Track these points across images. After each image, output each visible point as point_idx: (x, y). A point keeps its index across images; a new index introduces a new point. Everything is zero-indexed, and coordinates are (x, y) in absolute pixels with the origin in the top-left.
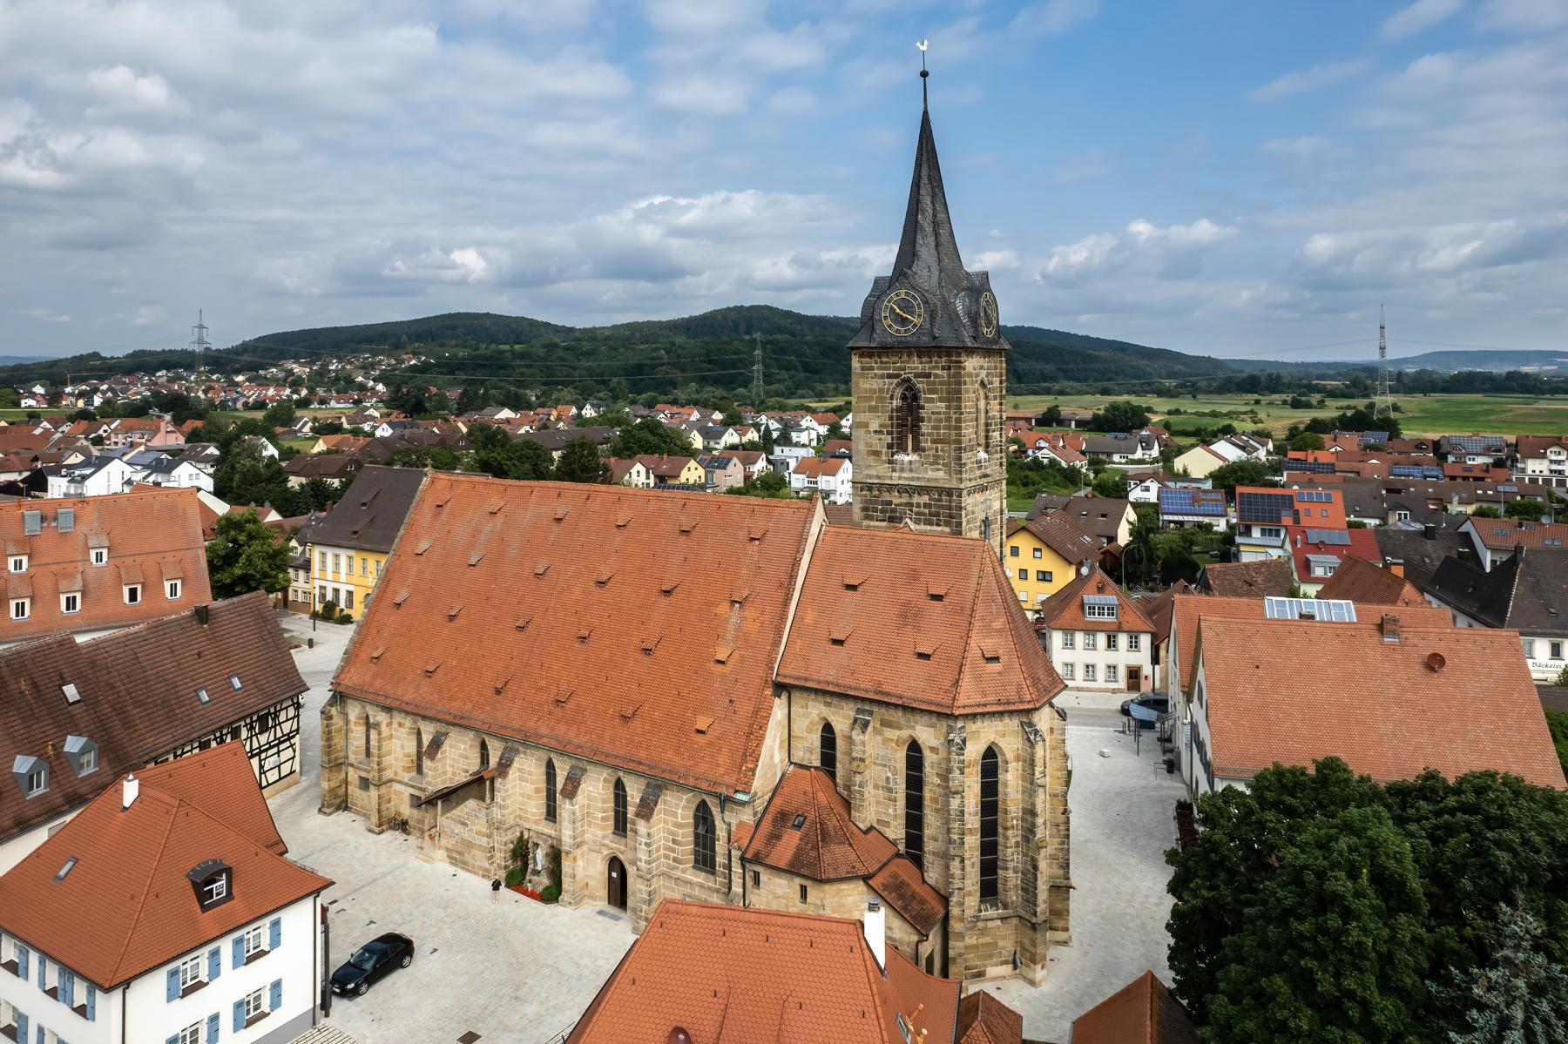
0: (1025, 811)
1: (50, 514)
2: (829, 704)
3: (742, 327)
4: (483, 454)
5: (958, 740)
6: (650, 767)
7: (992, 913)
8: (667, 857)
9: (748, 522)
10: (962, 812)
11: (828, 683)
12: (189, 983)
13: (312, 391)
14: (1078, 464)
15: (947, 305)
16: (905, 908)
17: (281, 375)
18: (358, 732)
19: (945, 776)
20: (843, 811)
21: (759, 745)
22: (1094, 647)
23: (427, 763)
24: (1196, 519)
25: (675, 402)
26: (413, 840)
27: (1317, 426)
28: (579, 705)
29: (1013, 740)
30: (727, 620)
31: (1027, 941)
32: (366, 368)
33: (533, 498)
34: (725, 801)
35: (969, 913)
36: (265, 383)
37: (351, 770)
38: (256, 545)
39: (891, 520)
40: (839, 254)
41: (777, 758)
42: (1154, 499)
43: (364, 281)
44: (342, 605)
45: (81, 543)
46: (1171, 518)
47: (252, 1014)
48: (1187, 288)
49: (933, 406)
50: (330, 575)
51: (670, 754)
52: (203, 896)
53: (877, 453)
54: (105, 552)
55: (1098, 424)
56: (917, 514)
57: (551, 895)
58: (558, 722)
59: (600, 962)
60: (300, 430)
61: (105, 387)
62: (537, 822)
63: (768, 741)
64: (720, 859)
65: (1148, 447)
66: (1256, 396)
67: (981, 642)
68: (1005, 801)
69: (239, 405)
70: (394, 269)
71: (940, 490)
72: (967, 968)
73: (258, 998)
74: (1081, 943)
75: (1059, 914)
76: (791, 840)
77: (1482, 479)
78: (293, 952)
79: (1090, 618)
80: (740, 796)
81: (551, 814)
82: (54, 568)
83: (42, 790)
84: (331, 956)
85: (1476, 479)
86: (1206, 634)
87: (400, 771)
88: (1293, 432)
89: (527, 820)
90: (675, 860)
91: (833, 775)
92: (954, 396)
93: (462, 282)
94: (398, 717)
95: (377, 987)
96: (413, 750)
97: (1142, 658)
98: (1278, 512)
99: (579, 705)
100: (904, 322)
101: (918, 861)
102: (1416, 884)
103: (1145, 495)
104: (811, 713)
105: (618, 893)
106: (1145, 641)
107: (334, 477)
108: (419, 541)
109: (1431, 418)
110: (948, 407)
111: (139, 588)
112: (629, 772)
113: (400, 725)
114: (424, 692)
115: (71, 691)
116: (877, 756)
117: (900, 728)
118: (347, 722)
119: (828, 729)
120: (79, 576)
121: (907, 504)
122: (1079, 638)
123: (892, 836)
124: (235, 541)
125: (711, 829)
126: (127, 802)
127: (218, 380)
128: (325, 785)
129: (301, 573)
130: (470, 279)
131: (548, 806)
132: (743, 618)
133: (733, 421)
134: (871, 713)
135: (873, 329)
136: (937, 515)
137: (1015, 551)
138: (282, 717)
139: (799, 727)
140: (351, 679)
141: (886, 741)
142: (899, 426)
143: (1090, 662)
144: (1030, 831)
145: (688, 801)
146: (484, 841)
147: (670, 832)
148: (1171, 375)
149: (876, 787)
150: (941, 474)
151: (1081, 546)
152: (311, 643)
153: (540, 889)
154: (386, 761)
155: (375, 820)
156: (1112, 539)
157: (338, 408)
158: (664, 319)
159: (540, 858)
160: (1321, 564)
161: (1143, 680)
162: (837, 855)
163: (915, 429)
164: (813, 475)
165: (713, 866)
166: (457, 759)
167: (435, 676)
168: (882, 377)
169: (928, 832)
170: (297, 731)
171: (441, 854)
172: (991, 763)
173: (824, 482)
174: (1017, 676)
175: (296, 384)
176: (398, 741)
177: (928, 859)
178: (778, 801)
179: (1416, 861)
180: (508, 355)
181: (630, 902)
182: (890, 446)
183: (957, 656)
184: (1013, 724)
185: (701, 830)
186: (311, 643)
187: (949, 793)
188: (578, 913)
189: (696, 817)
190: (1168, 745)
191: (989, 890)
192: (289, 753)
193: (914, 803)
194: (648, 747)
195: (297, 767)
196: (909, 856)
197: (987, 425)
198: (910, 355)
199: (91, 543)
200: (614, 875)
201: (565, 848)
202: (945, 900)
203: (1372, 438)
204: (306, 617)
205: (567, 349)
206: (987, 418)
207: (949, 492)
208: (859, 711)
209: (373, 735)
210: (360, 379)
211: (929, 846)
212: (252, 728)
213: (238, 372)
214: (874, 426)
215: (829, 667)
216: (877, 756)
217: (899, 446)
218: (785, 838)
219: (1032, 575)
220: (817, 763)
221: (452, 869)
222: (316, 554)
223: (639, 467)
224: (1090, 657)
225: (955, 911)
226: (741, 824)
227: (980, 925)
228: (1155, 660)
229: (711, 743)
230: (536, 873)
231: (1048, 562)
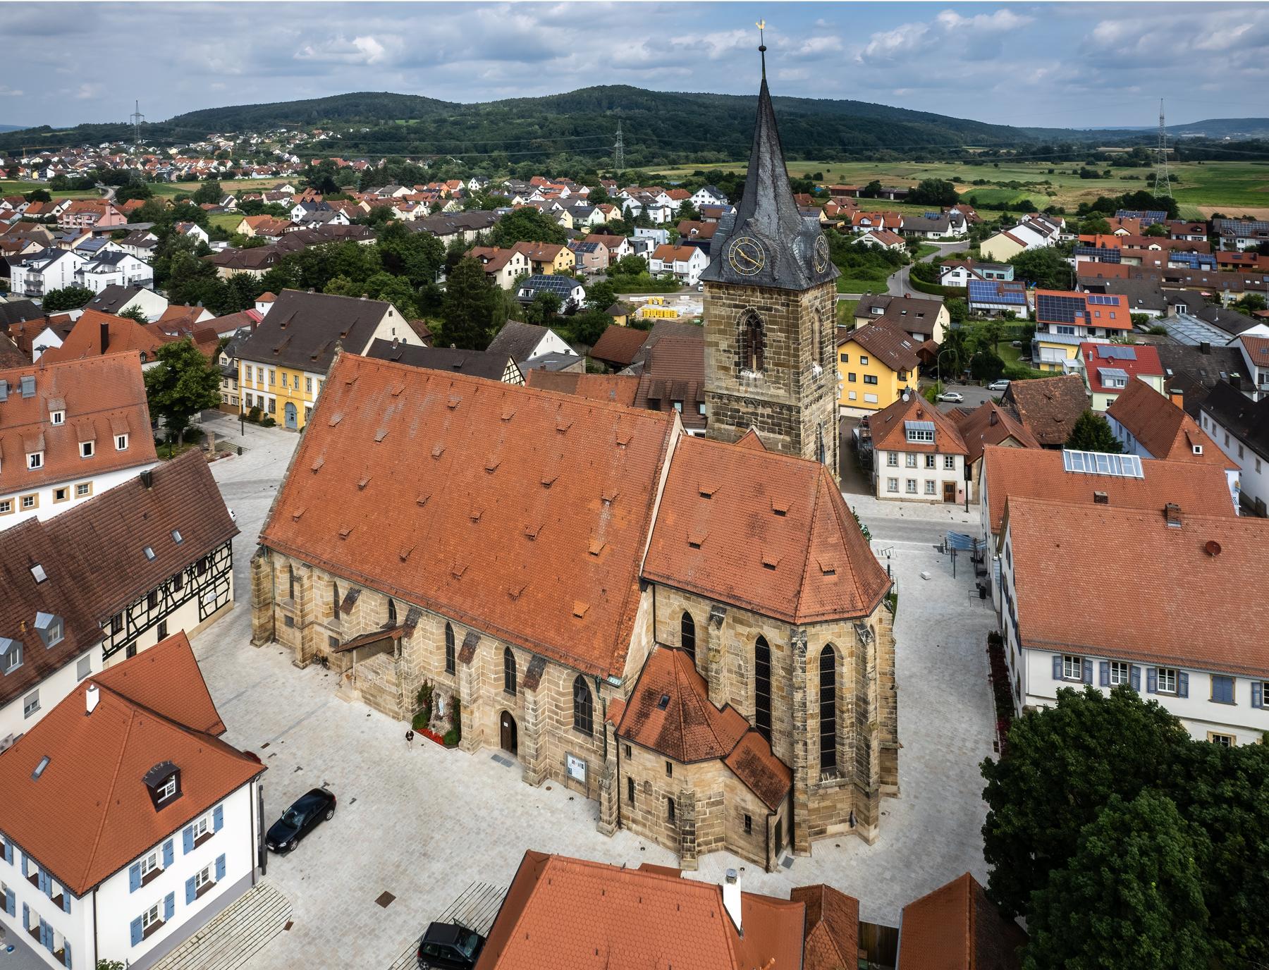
0: (858, 698)
1: (15, 382)
2: (688, 599)
3: (605, 103)
4: (384, 245)
5: (800, 644)
6: (536, 645)
7: (831, 781)
8: (551, 718)
9: (615, 427)
10: (804, 704)
11: (688, 583)
12: (148, 872)
13: (236, 163)
14: (896, 245)
15: (784, 249)
16: (756, 785)
17: (209, 148)
18: (283, 580)
19: (790, 670)
20: (701, 691)
21: (629, 635)
22: (915, 466)
23: (342, 615)
24: (1000, 307)
25: (547, 174)
26: (333, 676)
27: (1104, 206)
29: (848, 639)
31: (861, 804)
32: (283, 142)
33: (430, 386)
34: (599, 683)
35: (811, 782)
36: (195, 155)
37: (277, 609)
38: (191, 371)
39: (739, 425)
40: (688, 39)
41: (644, 641)
42: (963, 284)
43: (276, 62)
44: (266, 410)
45: (42, 405)
46: (979, 306)
47: (201, 885)
48: (989, 67)
49: (774, 335)
50: (255, 385)
51: (552, 634)
52: (155, 796)
53: (726, 369)
54: (62, 414)
55: (912, 198)
56: (762, 422)
57: (452, 739)
59: (496, 813)
60: (226, 206)
61: (56, 159)
62: (439, 674)
63: (636, 630)
64: (597, 727)
65: (959, 225)
66: (1049, 165)
67: (820, 557)
68: (841, 689)
69: (173, 178)
70: (304, 53)
71: (782, 406)
72: (810, 827)
73: (205, 871)
74: (908, 796)
75: (889, 771)
76: (658, 718)
77: (1251, 266)
78: (236, 824)
79: (911, 441)
80: (612, 680)
81: (451, 668)
82: (19, 430)
83: (18, 665)
84: (265, 807)
85: (1244, 265)
86: (1013, 513)
87: (320, 615)
88: (1083, 210)
89: (430, 671)
91: (692, 655)
92: (792, 328)
93: (363, 64)
94: (317, 572)
95: (305, 841)
96: (331, 599)
97: (957, 475)
98: (1072, 314)
99: (472, 580)
100: (748, 264)
101: (767, 735)
102: (1197, 895)
103: (956, 279)
104: (672, 606)
105: (510, 738)
106: (959, 462)
107: (256, 268)
108: (331, 414)
109: (1207, 190)
110: (787, 338)
111: (93, 443)
112: (519, 647)
113: (319, 578)
114: (340, 552)
115: (38, 572)
116: (730, 647)
117: (750, 626)
118: (274, 570)
119: (687, 617)
120: (41, 437)
121: (752, 414)
122: (902, 458)
123: (744, 713)
124: (173, 367)
125: (588, 699)
126: (90, 708)
127: (154, 153)
128: (256, 622)
129: (230, 381)
130: (370, 61)
131: (448, 661)
132: (613, 515)
133: (598, 199)
134: (724, 611)
135: (721, 267)
136: (779, 425)
137: (845, 358)
138: (218, 558)
139: (663, 613)
140: (276, 535)
141: (738, 635)
142: (745, 347)
143: (911, 477)
144: (862, 716)
145: (568, 675)
146: (394, 689)
147: (553, 699)
148: (976, 143)
149: (730, 671)
150: (781, 392)
151: (901, 352)
152: (240, 451)
153: (442, 733)
154: (308, 608)
155: (299, 656)
156: (928, 336)
157: (259, 177)
158: (538, 96)
159: (442, 706)
160: (1110, 377)
161: (957, 494)
162: (698, 734)
163: (760, 346)
165: (591, 729)
166: (369, 614)
167: (348, 540)
168: (729, 306)
169: (775, 714)
170: (231, 567)
171: (356, 694)
172: (828, 658)
173: (678, 266)
174: (850, 587)
175: (222, 157)
176: (318, 593)
177: (775, 736)
178: (645, 679)
179: (1197, 859)
180: (404, 131)
181: (520, 749)
182: (737, 364)
183: (798, 569)
184: (848, 627)
185: (580, 700)
186: (240, 451)
187: (792, 688)
188: (475, 758)
189: (575, 687)
190: (980, 566)
191: (829, 761)
192: (225, 586)
193: (763, 686)
194: (533, 625)
195: (231, 597)
196: (759, 729)
197: (821, 343)
198: (753, 290)
199: (51, 405)
200: (506, 725)
201: (463, 703)
202: (791, 773)
203: (1154, 217)
204: (235, 418)
205: (455, 123)
206: (821, 337)
207: (790, 408)
208: (714, 608)
209: (296, 587)
210: (277, 152)
211: (776, 725)
212: (192, 572)
213: (171, 145)
214: (724, 345)
215: (688, 567)
216: (730, 647)
217: (744, 364)
218: (653, 716)
219: (860, 379)
220: (679, 644)
222: (242, 367)
223: (518, 255)
224: (911, 473)
225: (799, 785)
226: (614, 701)
227: (821, 792)
228: (968, 477)
229: (587, 628)
230: (439, 718)
231: (874, 368)
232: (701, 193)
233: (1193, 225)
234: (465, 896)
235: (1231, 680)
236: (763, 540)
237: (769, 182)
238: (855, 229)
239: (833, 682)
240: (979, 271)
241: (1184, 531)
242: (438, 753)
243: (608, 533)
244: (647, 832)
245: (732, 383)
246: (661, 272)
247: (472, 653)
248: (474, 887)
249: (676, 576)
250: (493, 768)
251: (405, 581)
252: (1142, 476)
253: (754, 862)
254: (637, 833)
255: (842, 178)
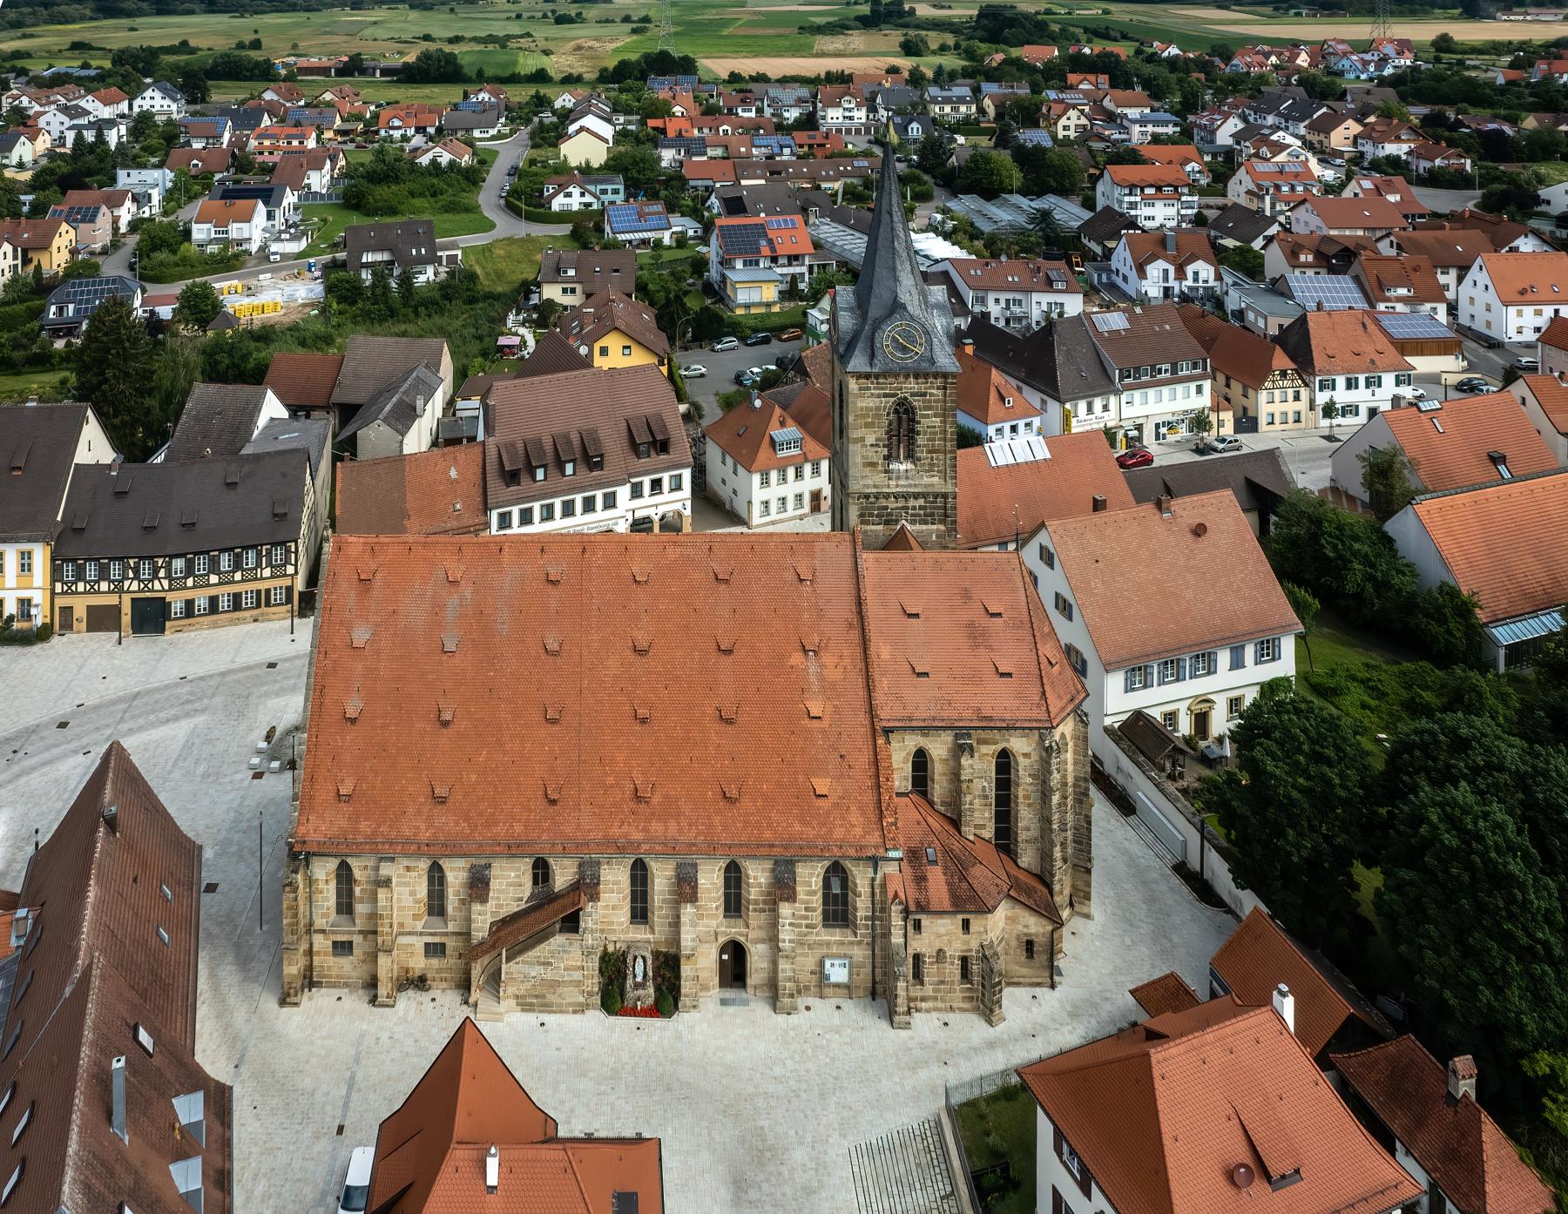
2: (926, 735)
28: (667, 797)
30: (805, 670)
31: (1080, 884)
39: (887, 523)
51: (797, 827)
53: (873, 465)
58: (648, 821)
59: (789, 1063)
71: (936, 495)
79: (780, 454)
90: (807, 926)
99: (667, 797)
100: (904, 349)
103: (567, 200)
104: (912, 742)
110: (944, 422)
132: (822, 666)
134: (969, 736)
153: (650, 1001)
163: (912, 433)
164: (222, 223)
168: (878, 396)
171: (508, 1003)
173: (236, 230)
194: (770, 826)
198: (907, 377)
207: (945, 496)
214: (871, 439)
221: (532, 1019)
229: (836, 805)
232: (149, 93)
233: (741, 95)
234: (856, 1169)
235: (1243, 647)
236: (991, 648)
237: (904, 255)
238: (382, 133)
239: (926, 770)
240: (591, 188)
241: (1174, 517)
242: (663, 1029)
243: (823, 689)
244: (940, 1004)
245: (879, 478)
246: (211, 242)
247: (695, 888)
248: (854, 1154)
249: (917, 714)
250: (735, 1016)
251: (568, 829)
252: (1048, 456)
253: (1038, 985)
254: (928, 1011)
255: (295, 46)
